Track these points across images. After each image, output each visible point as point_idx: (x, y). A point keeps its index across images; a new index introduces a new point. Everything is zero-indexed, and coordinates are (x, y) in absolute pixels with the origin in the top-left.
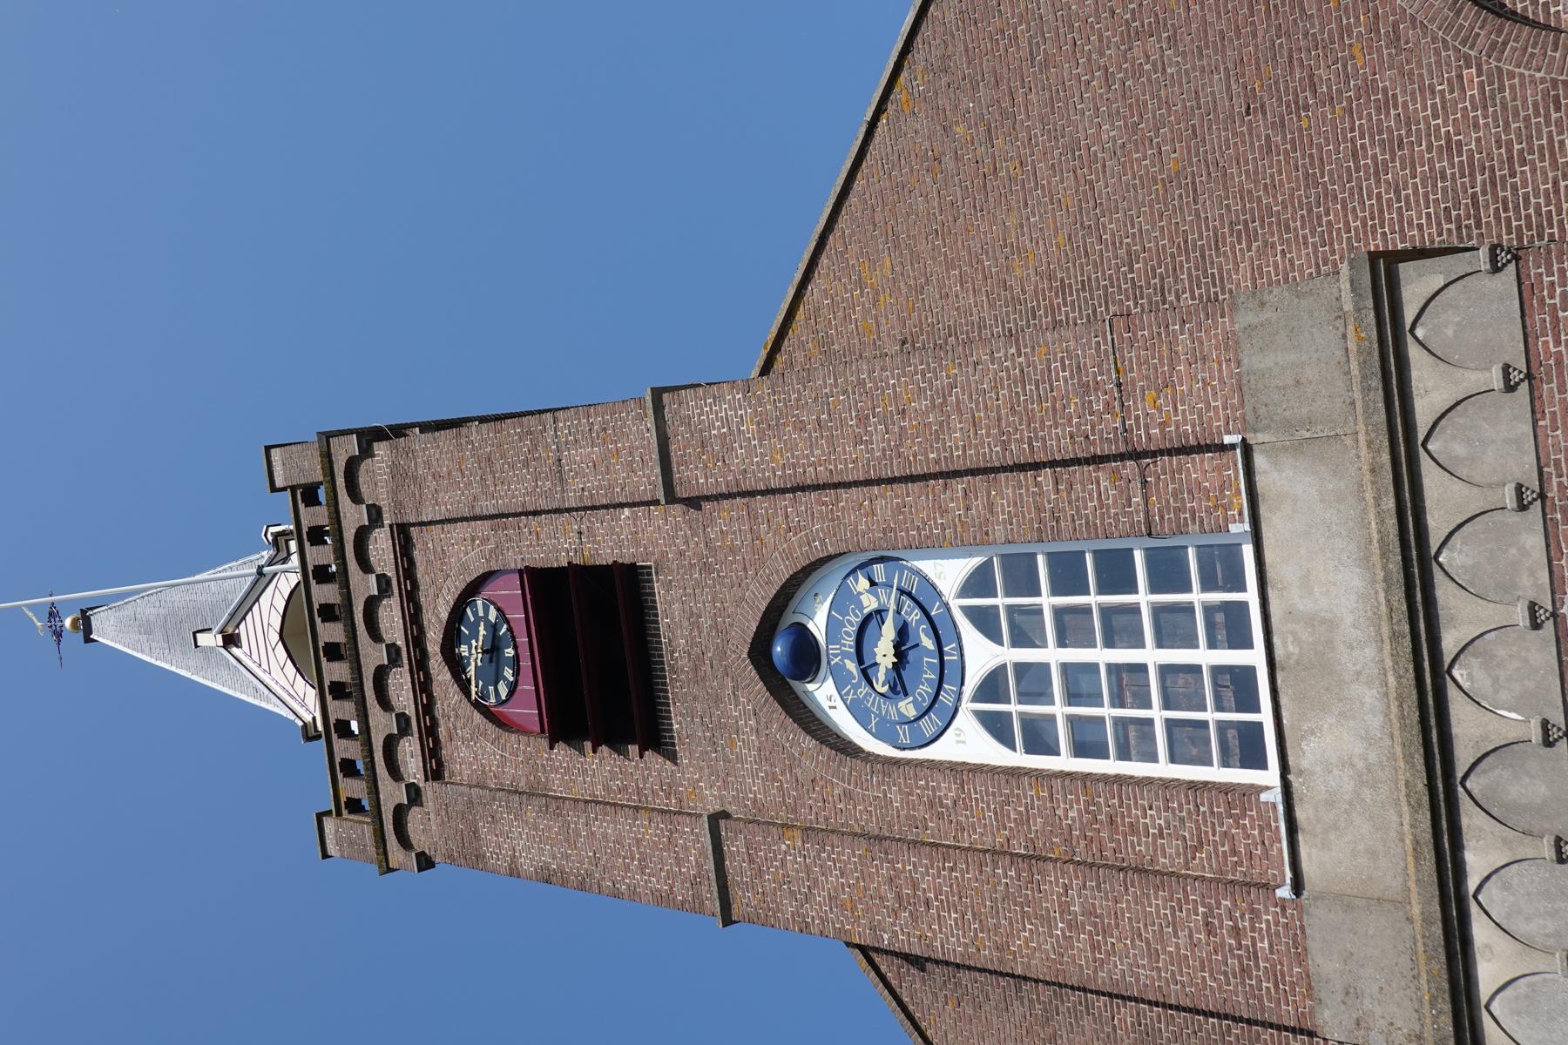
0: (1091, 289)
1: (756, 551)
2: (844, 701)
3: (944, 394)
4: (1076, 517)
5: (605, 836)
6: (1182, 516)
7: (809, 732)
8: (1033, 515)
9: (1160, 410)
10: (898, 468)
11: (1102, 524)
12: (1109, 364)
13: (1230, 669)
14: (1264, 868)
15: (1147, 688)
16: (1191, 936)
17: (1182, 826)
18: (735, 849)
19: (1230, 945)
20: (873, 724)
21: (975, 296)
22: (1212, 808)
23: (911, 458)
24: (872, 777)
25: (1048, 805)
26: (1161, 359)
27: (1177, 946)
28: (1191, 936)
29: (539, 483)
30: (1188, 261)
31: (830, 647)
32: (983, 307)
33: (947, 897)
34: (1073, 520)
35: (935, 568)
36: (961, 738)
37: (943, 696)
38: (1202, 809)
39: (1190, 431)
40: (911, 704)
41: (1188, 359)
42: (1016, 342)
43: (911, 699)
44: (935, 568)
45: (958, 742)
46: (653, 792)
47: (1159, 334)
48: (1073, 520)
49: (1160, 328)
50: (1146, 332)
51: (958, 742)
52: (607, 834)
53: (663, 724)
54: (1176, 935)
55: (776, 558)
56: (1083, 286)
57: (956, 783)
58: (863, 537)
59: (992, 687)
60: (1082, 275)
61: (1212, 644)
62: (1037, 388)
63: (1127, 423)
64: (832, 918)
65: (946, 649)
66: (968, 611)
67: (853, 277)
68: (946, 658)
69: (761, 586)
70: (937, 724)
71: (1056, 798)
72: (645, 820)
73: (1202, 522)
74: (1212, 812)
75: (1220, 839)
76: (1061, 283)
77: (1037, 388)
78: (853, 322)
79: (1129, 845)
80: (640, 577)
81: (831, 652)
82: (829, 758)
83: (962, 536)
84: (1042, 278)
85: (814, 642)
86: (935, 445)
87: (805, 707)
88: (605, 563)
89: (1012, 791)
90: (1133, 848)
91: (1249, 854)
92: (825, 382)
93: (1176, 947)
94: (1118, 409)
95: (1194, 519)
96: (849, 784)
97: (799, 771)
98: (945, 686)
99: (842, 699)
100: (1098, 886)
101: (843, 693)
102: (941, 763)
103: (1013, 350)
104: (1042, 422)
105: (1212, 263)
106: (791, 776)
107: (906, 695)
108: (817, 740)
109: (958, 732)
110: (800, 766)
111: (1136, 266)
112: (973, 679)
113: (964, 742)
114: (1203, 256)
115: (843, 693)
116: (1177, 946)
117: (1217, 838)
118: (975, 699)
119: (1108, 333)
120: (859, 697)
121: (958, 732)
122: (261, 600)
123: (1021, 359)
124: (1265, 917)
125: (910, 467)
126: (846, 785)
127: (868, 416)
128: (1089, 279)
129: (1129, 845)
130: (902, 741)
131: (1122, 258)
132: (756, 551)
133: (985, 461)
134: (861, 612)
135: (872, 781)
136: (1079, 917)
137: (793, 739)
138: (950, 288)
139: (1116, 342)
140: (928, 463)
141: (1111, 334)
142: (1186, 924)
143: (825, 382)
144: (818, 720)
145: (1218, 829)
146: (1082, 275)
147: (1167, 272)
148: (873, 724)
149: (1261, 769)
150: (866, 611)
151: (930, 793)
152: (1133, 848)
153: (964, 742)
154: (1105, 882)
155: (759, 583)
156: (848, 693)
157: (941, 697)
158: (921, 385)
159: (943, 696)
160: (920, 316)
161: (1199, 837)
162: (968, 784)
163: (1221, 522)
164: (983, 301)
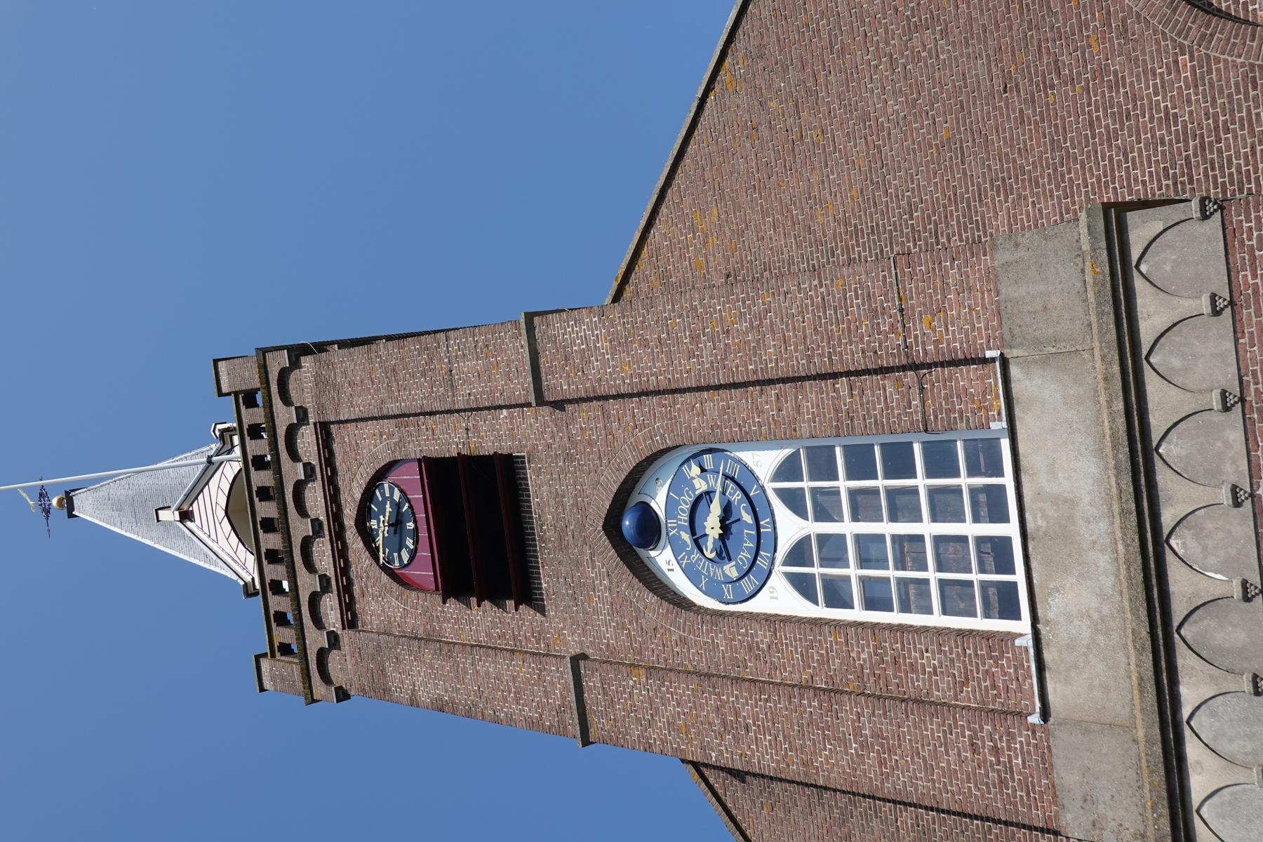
0: (879, 233)
1: (609, 444)
2: (680, 565)
3: (760, 318)
4: (867, 417)
5: (487, 673)
6: (952, 416)
7: (652, 589)
8: (832, 415)
9: (934, 330)
10: (724, 377)
11: (888, 422)
12: (894, 294)
13: (991, 539)
14: (1018, 699)
15: (924, 555)
16: (959, 755)
17: (952, 665)
18: (592, 684)
19: (991, 761)
20: (703, 583)
21: (785, 239)
22: (977, 651)
23: (734, 369)
24: (702, 626)
25: (844, 648)
26: (935, 289)
27: (948, 762)
28: (959, 755)
29: (435, 389)
30: (957, 210)
31: (669, 521)
32: (791, 247)
33: (763, 723)
34: (865, 419)
35: (753, 458)
36: (774, 595)
37: (759, 561)
38: (968, 652)
39: (958, 347)
40: (734, 567)
41: (957, 289)
42: (818, 275)
43: (734, 563)
44: (753, 458)
45: (772, 598)
46: (526, 638)
47: (934, 269)
48: (865, 419)
49: (934, 264)
50: (923, 268)
51: (772, 598)
52: (489, 672)
53: (534, 583)
54: (947, 754)
55: (625, 449)
56: (873, 230)
57: (770, 631)
58: (695, 432)
59: (799, 553)
60: (872, 222)
61: (976, 519)
62: (836, 312)
63: (908, 341)
64: (670, 739)
65: (762, 523)
66: (780, 492)
67: (687, 224)
68: (762, 530)
69: (613, 472)
70: (755, 583)
71: (851, 643)
72: (520, 661)
73: (968, 420)
74: (976, 655)
75: (983, 676)
76: (855, 228)
77: (836, 312)
78: (687, 259)
79: (909, 681)
80: (516, 465)
81: (669, 525)
82: (668, 611)
83: (775, 432)
84: (839, 224)
85: (655, 517)
86: (753, 359)
87: (649, 569)
88: (487, 454)
89: (815, 637)
90: (913, 683)
91: (1006, 688)
92: (664, 307)
93: (947, 763)
94: (900, 330)
95: (962, 418)
96: (684, 632)
97: (643, 621)
98: (761, 553)
99: (678, 563)
100: (885, 714)
101: (679, 558)
102: (758, 615)
103: (816, 282)
104: (840, 340)
105: (976, 212)
106: (637, 625)
107: (730, 560)
108: (658, 596)
109: (771, 590)
110: (644, 617)
111: (915, 214)
112: (784, 547)
113: (776, 598)
114: (969, 206)
115: (679, 558)
116: (948, 762)
117: (980, 676)
118: (786, 563)
119: (893, 269)
120: (692, 562)
121: (771, 590)
122: (210, 483)
123: (823, 290)
124: (1019, 739)
125: (733, 377)
126: (681, 633)
127: (699, 335)
128: (877, 225)
129: (909, 681)
130: (727, 597)
131: (904, 208)
132: (609, 444)
133: (793, 371)
134: (694, 493)
135: (703, 629)
136: (869, 739)
137: (639, 595)
138: (766, 232)
139: (899, 276)
140: (747, 373)
141: (895, 269)
142: (955, 745)
143: (664, 307)
144: (659, 580)
145: (981, 668)
146: (872, 222)
147: (940, 219)
148: (703, 583)
149: (1015, 620)
150: (697, 493)
151: (749, 639)
152: (913, 683)
153: (776, 598)
154: (890, 711)
155: (611, 469)
156: (683, 559)
157: (758, 562)
158: (742, 310)
159: (759, 561)
160: (741, 255)
161: (966, 674)
162: (780, 632)
163: (983, 420)
164: (792, 242)
